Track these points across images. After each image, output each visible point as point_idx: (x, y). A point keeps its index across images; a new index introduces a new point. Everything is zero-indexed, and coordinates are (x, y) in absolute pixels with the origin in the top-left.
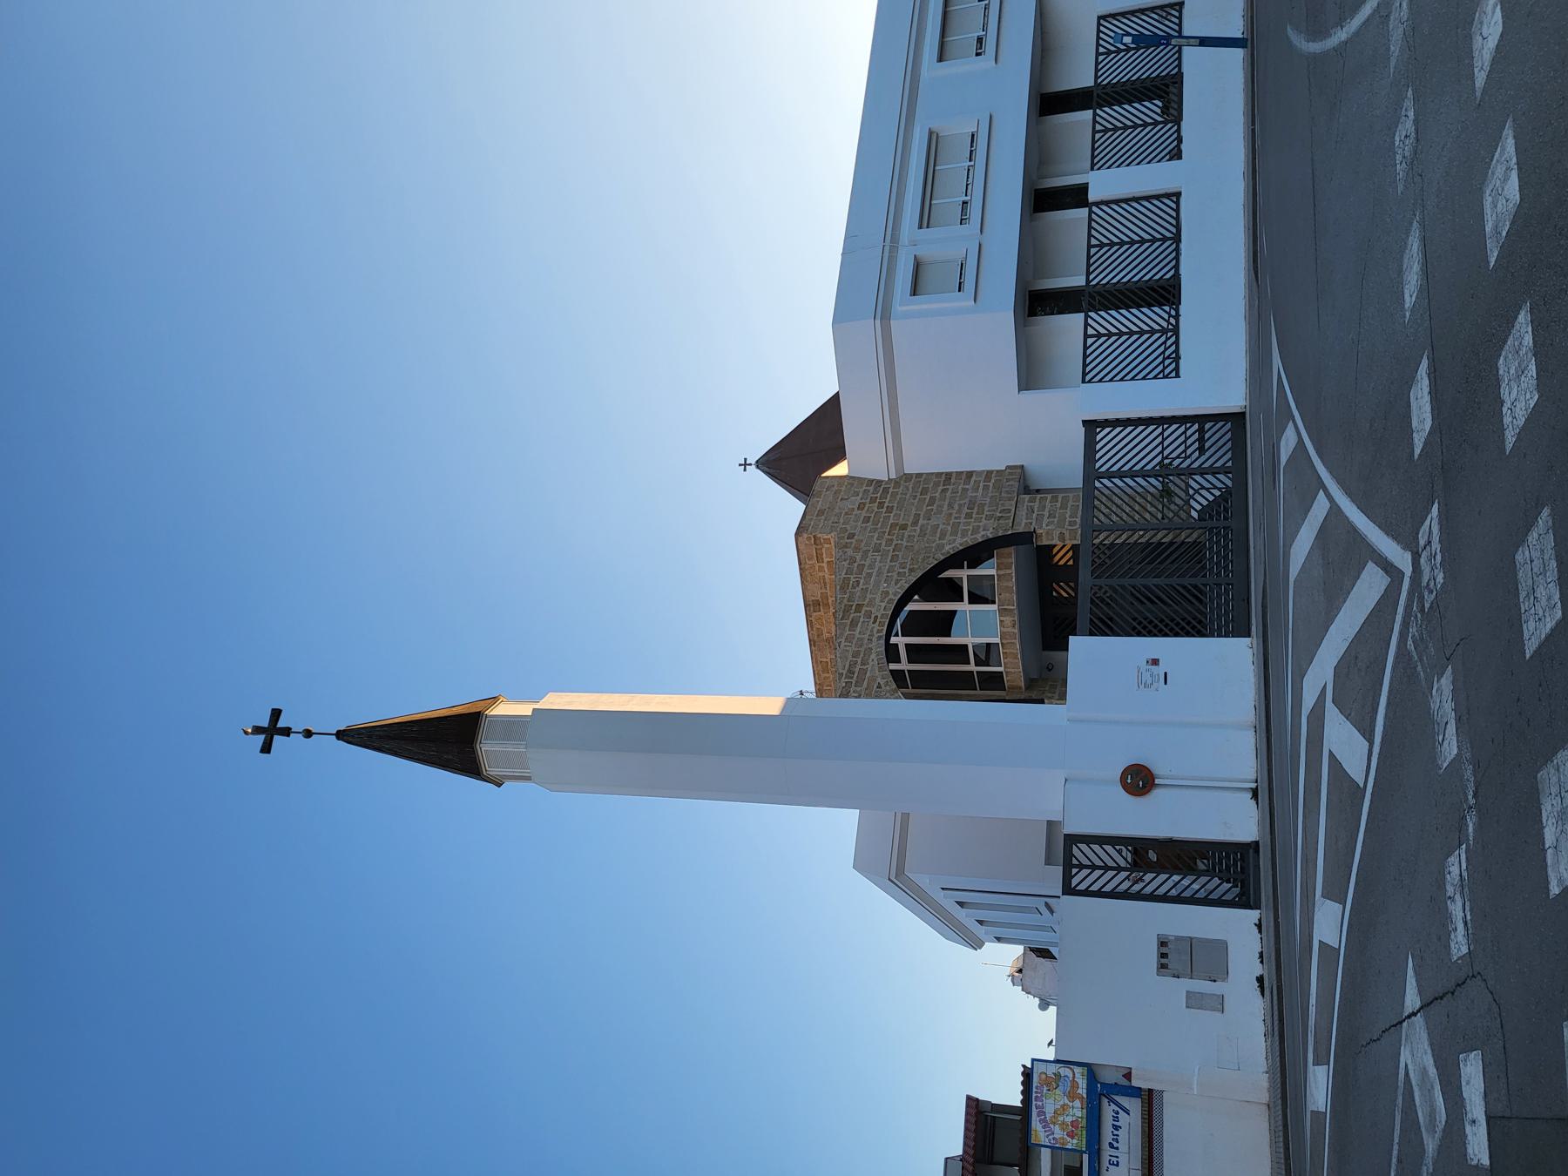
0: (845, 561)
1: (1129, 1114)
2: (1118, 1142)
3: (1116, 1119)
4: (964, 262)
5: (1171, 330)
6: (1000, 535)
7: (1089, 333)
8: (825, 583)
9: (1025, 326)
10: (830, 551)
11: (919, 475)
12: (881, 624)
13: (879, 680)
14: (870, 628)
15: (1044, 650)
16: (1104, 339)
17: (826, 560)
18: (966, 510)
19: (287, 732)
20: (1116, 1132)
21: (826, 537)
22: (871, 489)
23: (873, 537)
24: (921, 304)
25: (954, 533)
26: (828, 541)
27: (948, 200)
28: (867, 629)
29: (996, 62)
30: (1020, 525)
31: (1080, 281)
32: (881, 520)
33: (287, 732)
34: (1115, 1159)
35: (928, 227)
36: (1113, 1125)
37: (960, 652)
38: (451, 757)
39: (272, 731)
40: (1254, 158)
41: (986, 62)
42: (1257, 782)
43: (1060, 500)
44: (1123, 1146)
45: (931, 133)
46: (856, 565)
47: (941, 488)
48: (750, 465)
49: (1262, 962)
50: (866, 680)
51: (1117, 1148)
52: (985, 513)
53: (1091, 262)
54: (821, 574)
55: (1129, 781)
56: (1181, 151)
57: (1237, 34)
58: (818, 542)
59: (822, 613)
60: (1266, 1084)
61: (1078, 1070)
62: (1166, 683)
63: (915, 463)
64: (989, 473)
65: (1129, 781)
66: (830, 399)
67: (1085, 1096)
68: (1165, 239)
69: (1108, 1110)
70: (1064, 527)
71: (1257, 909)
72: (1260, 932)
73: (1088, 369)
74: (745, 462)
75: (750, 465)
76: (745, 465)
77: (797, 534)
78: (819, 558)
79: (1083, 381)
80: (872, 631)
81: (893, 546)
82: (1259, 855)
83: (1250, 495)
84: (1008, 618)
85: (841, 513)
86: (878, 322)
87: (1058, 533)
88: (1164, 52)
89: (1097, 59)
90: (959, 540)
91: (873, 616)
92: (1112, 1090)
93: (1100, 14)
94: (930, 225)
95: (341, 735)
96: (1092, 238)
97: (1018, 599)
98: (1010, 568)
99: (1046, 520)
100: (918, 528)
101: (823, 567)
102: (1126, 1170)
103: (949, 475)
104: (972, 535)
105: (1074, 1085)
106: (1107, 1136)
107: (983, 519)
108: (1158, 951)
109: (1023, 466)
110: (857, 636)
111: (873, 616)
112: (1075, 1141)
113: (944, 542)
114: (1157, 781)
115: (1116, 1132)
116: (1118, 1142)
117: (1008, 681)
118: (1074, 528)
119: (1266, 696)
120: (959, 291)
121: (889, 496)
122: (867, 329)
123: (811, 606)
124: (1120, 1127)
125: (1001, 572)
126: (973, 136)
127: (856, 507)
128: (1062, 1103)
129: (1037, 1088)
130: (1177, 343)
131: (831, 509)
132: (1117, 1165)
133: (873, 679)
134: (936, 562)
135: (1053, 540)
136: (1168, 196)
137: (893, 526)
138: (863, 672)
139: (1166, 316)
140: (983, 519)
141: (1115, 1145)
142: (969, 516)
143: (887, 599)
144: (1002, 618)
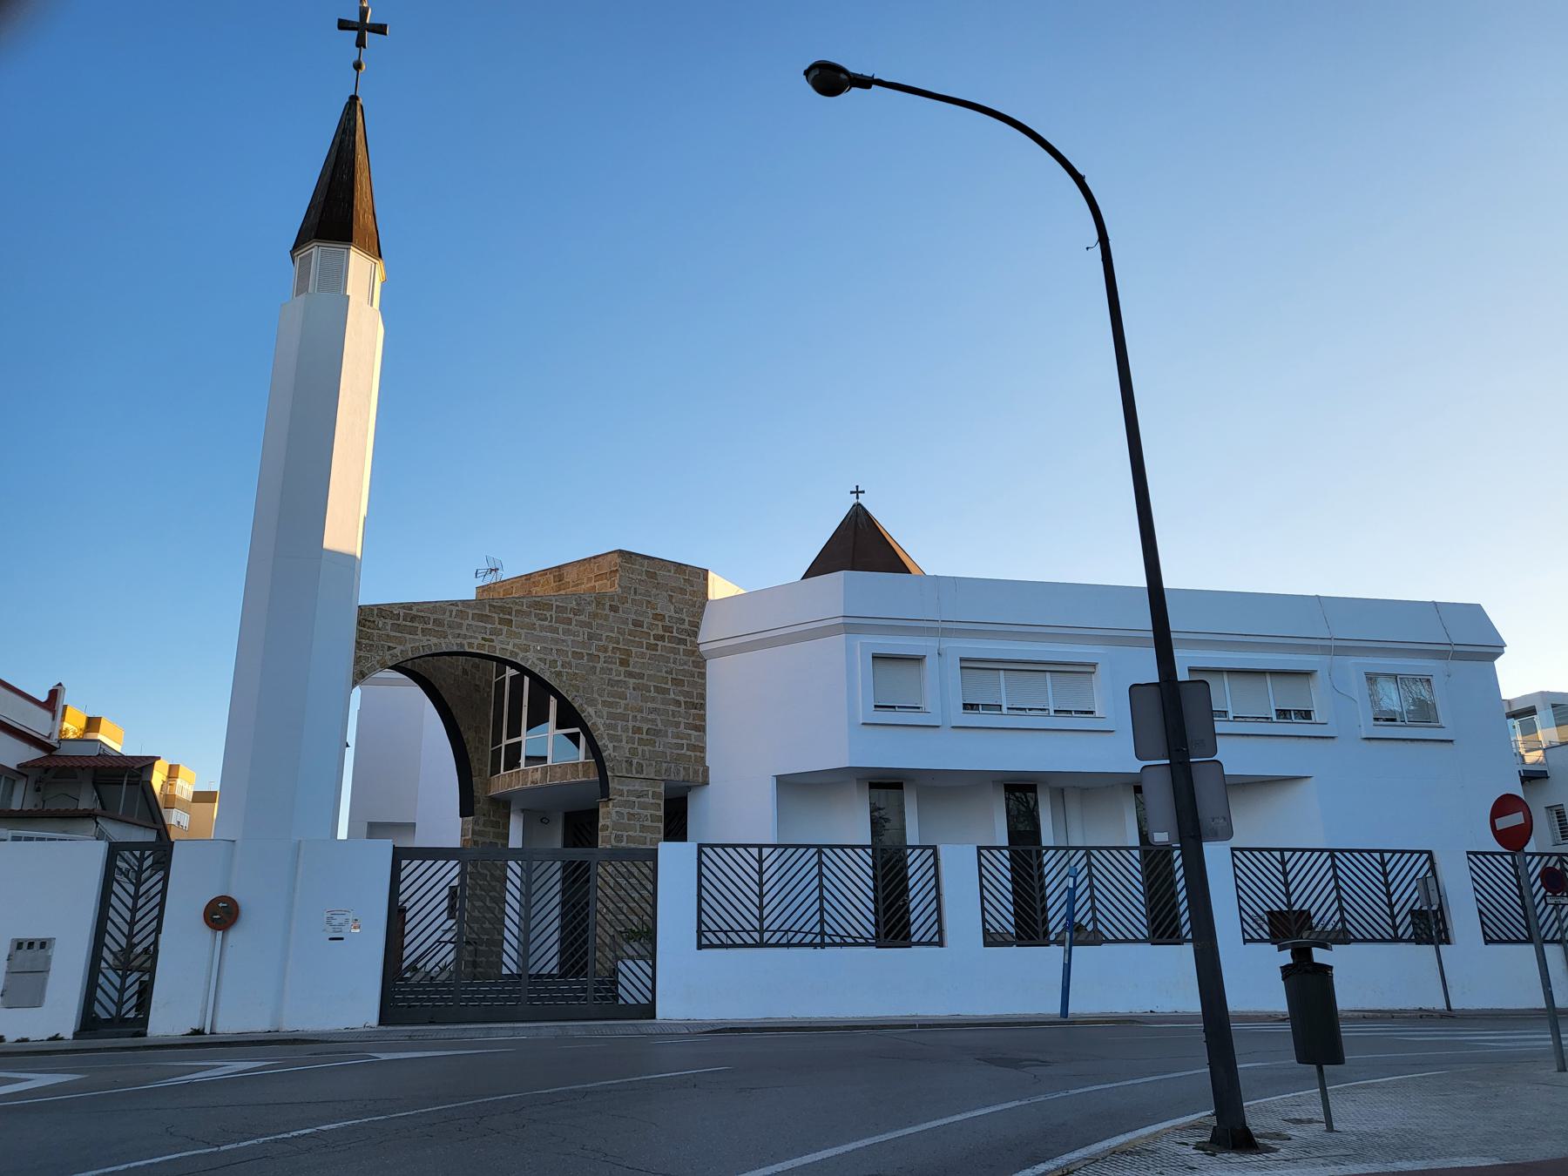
0: (578, 604)
4: (920, 710)
5: (761, 937)
6: (607, 764)
7: (764, 849)
8: (577, 585)
9: (858, 779)
10: (611, 587)
11: (703, 675)
12: (480, 646)
13: (400, 648)
14: (477, 635)
15: (565, 813)
16: (1280, 868)
17: (597, 584)
18: (645, 727)
19: (360, 43)
21: (616, 582)
22: (686, 626)
23: (612, 631)
24: (863, 666)
25: (611, 716)
27: (1002, 689)
28: (474, 632)
30: (619, 784)
31: (1047, 838)
32: (637, 639)
33: (360, 43)
35: (961, 668)
37: (515, 731)
39: (361, 28)
40: (838, 1028)
42: (211, 1033)
43: (654, 824)
45: (1094, 665)
46: (571, 616)
47: (682, 699)
48: (857, 498)
49: (18, 1041)
50: (400, 635)
52: (640, 748)
53: (1364, 854)
54: (585, 581)
55: (221, 905)
56: (1048, 945)
57: (1070, 1011)
58: (613, 574)
59: (553, 584)
62: (330, 939)
63: (716, 671)
64: (703, 749)
65: (221, 905)
68: (1395, 928)
70: (613, 829)
72: (50, 1039)
73: (1104, 852)
74: (861, 492)
75: (857, 498)
76: (857, 492)
77: (621, 553)
78: (599, 577)
79: (1468, 853)
80: (471, 637)
81: (596, 653)
82: (132, 1037)
83: (472, 1026)
84: (540, 776)
85: (650, 596)
86: (841, 620)
89: (1376, 851)
90: (600, 722)
91: (494, 637)
94: (965, 671)
95: (354, 99)
96: (1390, 854)
97: (558, 785)
98: (584, 776)
99: (625, 811)
100: (622, 678)
101: (591, 582)
103: (702, 706)
104: (608, 734)
107: (630, 745)
108: (36, 940)
109: (708, 784)
110: (465, 623)
111: (494, 637)
113: (600, 706)
114: (220, 933)
118: (613, 840)
119: (224, 1043)
120: (876, 706)
121: (674, 645)
123: (558, 572)
125: (580, 767)
126: (1092, 712)
127: (658, 611)
130: (746, 945)
131: (657, 586)
133: (401, 641)
134: (569, 699)
135: (603, 819)
136: (940, 932)
137: (628, 653)
138: (413, 631)
139: (806, 929)
140: (630, 745)
142: (638, 730)
143: (517, 651)
144: (540, 770)
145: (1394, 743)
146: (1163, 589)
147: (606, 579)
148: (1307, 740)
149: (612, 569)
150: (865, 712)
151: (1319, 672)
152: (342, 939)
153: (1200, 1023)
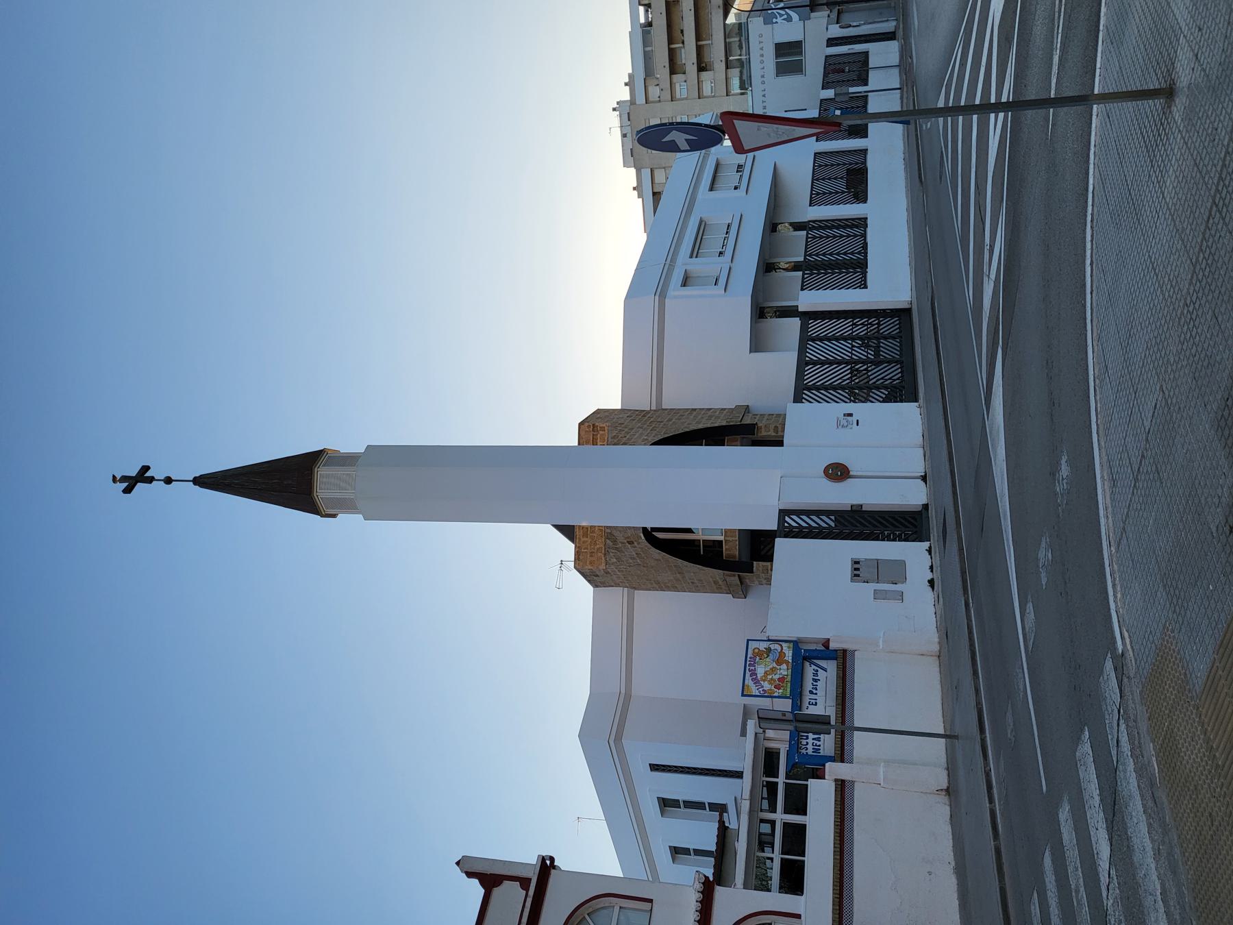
1: (826, 671)
2: (816, 690)
3: (816, 674)
20: (815, 683)
21: (602, 425)
26: (603, 429)
29: (747, 194)
34: (814, 701)
35: (696, 257)
36: (813, 679)
38: (290, 482)
41: (741, 192)
44: (821, 692)
45: (701, 221)
51: (816, 694)
55: (830, 472)
56: (867, 244)
60: (937, 640)
61: (784, 645)
65: (830, 472)
66: (632, 281)
67: (790, 661)
69: (809, 670)
71: (927, 541)
79: (810, 206)
86: (657, 297)
87: (773, 426)
88: (837, 369)
92: (810, 657)
93: (816, 151)
94: (699, 256)
102: (823, 707)
105: (782, 654)
106: (808, 685)
112: (781, 691)
115: (815, 683)
116: (816, 690)
117: (726, 549)
120: (715, 285)
122: (650, 302)
124: (819, 680)
126: (729, 226)
128: (771, 666)
129: (750, 658)
132: (816, 704)
135: (769, 431)
141: (815, 691)
145: (751, 185)
146: (622, 410)
147: (597, 435)
148: (754, 167)
149: (591, 430)
150: (719, 290)
151: (719, 157)
152: (858, 421)
153: (907, 107)
